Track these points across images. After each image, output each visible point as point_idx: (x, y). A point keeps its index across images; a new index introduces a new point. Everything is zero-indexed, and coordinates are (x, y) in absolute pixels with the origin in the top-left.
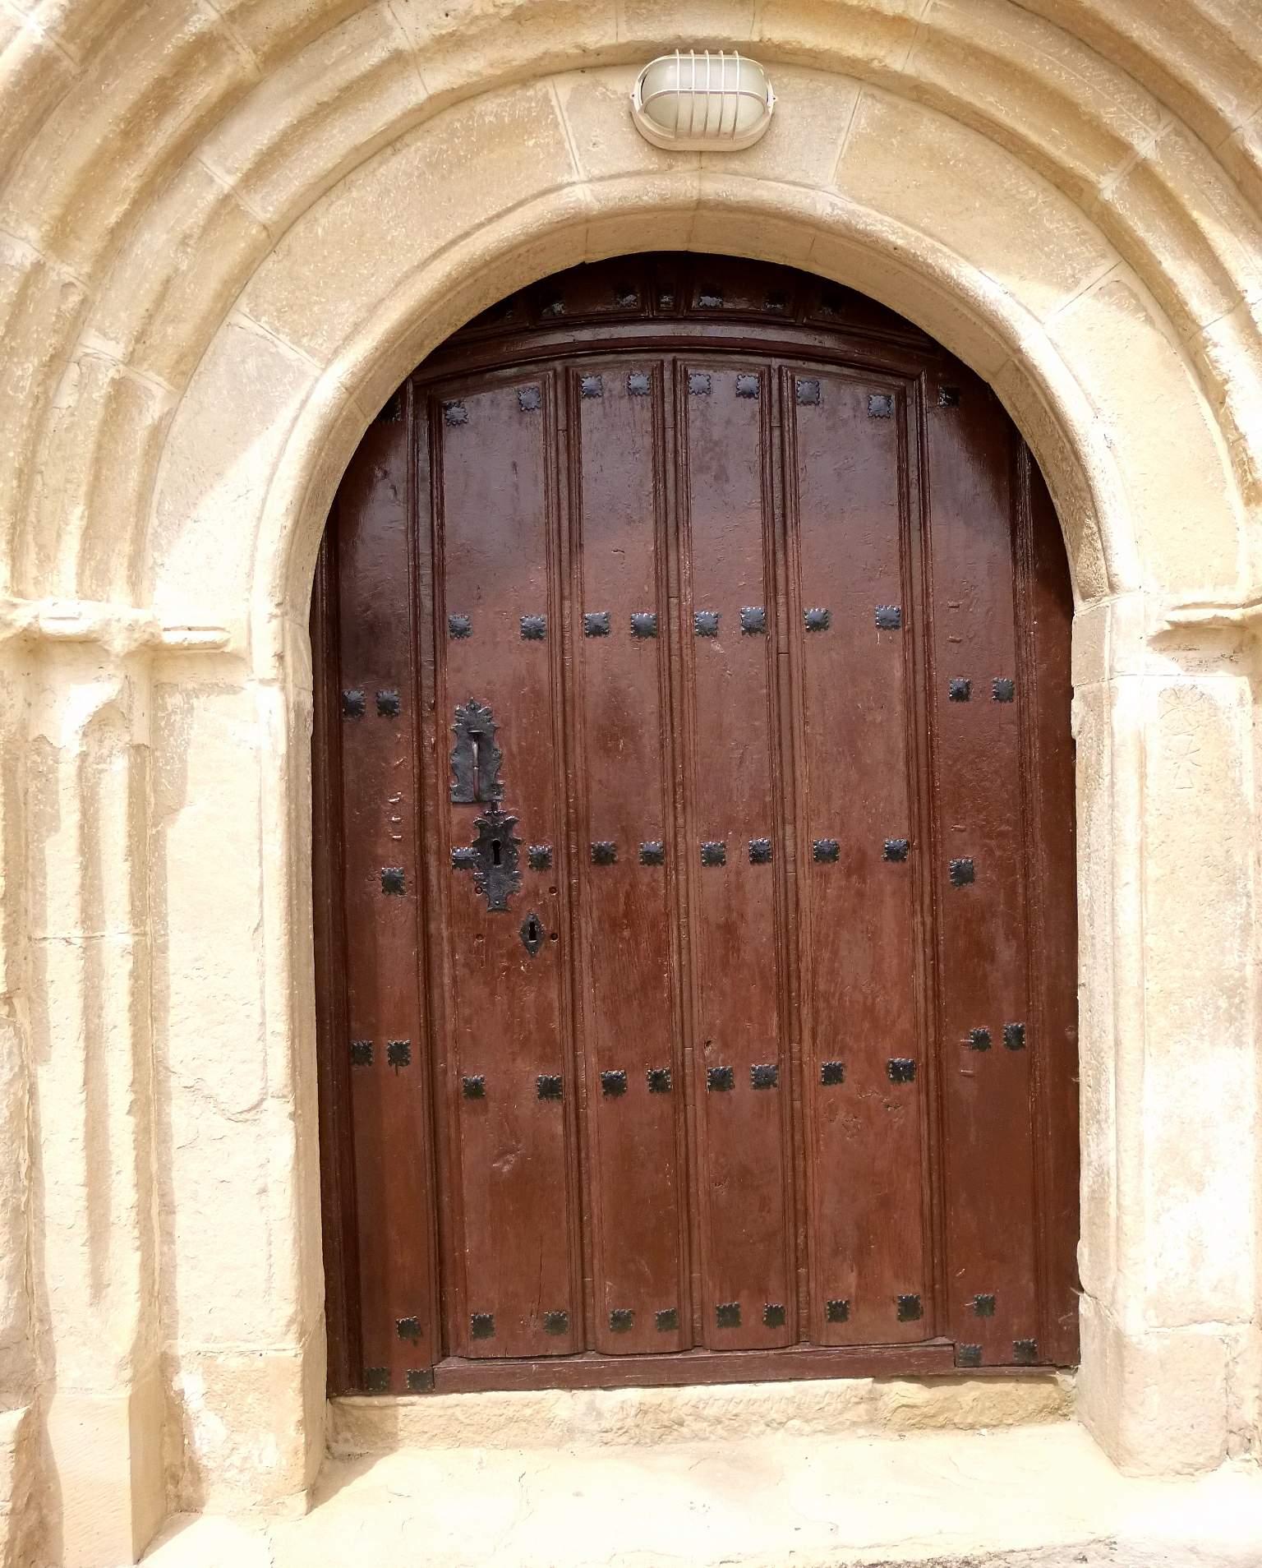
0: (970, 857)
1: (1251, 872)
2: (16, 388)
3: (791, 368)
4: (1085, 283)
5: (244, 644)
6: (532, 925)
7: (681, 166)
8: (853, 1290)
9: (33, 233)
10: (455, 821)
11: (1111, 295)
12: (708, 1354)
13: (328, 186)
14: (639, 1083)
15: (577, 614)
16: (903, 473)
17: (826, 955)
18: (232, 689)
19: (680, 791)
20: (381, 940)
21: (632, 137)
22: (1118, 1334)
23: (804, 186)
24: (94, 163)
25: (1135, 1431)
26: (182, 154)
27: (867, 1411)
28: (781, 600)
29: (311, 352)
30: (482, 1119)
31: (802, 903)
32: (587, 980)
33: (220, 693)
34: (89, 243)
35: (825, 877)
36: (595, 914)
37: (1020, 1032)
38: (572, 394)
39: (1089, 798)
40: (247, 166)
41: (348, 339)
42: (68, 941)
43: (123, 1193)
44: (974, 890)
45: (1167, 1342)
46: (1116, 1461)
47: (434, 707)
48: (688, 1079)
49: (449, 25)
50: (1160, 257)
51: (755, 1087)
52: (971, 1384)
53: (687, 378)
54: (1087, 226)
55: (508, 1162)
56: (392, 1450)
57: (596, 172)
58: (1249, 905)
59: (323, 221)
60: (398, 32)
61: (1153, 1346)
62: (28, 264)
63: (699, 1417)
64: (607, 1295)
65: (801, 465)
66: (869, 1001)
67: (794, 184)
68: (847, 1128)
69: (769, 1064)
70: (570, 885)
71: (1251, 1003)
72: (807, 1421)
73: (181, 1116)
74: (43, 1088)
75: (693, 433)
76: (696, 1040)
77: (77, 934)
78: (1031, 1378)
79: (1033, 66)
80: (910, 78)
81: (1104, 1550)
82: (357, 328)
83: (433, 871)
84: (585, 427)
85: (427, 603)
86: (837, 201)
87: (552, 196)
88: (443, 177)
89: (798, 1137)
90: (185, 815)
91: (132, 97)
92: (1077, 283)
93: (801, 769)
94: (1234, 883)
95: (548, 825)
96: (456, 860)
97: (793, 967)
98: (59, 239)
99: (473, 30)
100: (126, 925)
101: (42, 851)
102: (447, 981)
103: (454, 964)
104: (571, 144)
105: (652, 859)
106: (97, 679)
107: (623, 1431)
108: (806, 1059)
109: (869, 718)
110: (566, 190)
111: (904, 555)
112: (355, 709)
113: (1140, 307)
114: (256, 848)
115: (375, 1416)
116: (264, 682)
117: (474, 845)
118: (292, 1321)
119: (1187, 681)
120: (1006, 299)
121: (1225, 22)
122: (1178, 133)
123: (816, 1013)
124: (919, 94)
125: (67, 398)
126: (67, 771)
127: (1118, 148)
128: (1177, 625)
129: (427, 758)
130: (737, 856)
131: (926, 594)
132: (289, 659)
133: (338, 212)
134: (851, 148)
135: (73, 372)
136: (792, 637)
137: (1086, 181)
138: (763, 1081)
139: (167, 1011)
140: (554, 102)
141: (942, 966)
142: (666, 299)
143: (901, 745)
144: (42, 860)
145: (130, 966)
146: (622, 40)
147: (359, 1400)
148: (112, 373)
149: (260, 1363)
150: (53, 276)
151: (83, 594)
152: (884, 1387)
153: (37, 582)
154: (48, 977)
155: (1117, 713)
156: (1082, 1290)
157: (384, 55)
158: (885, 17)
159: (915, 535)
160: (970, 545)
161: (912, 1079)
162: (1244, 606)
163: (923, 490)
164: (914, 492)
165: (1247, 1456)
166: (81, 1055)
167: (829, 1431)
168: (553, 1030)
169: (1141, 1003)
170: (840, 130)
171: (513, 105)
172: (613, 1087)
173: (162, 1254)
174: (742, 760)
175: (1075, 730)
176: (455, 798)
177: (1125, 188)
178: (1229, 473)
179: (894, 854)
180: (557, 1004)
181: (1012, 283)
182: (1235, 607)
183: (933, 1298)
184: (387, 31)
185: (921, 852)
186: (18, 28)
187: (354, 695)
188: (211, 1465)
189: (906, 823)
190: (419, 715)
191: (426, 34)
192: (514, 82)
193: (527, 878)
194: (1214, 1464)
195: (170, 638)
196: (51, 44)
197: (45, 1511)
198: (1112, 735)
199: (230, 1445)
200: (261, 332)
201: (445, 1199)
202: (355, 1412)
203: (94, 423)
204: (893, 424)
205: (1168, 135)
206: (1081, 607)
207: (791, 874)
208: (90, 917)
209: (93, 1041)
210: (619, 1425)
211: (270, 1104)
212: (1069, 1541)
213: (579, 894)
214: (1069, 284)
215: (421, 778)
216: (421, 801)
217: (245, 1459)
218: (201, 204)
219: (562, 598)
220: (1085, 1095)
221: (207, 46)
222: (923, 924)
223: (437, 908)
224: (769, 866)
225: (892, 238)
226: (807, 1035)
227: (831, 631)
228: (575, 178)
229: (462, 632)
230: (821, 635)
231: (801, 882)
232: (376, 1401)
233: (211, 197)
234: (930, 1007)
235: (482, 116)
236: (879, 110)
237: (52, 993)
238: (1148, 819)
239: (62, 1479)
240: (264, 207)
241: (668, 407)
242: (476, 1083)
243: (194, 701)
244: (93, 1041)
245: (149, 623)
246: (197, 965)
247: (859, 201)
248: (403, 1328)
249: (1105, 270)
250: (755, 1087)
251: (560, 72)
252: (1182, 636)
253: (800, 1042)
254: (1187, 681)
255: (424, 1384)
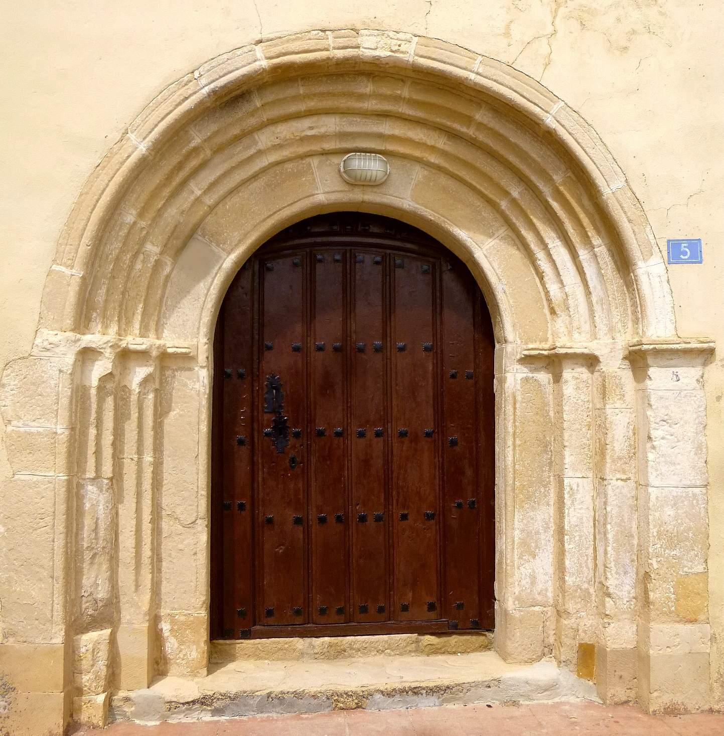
0: (455, 437)
1: (552, 444)
2: (124, 264)
3: (394, 254)
4: (496, 235)
5: (196, 353)
6: (293, 458)
7: (356, 190)
8: (411, 599)
9: (134, 212)
10: (266, 418)
11: (505, 239)
12: (356, 624)
13: (231, 192)
14: (332, 520)
15: (312, 342)
16: (434, 294)
17: (402, 472)
18: (190, 369)
19: (349, 409)
21: (339, 179)
22: (506, 611)
23: (400, 198)
24: (156, 189)
25: (511, 646)
26: (184, 183)
27: (416, 647)
28: (388, 339)
29: (224, 250)
30: (272, 532)
31: (394, 453)
32: (313, 479)
33: (185, 371)
34: (151, 214)
35: (402, 443)
36: (317, 455)
37: (473, 502)
38: (313, 261)
39: (499, 416)
40: (206, 187)
41: (237, 245)
42: (132, 459)
43: (147, 552)
44: (457, 449)
45: (522, 613)
46: (505, 659)
47: (258, 376)
48: (350, 518)
49: (278, 142)
50: (521, 230)
51: (375, 521)
52: (454, 636)
53: (356, 257)
54: (498, 216)
55: (281, 549)
56: (233, 661)
57: (326, 190)
58: (552, 455)
59: (229, 203)
60: (260, 143)
61: (517, 615)
62: (132, 222)
63: (352, 649)
64: (318, 600)
65: (396, 290)
66: (418, 490)
67: (396, 197)
68: (410, 538)
69: (380, 513)
70: (307, 444)
71: (552, 490)
72: (392, 651)
73: (165, 525)
74: (120, 512)
75: (358, 277)
76: (354, 503)
77: (135, 457)
78: (478, 634)
79: (478, 165)
80: (436, 164)
81: (496, 683)
82: (240, 241)
84: (317, 273)
85: (256, 337)
86: (410, 203)
87: (311, 198)
88: (272, 190)
89: (391, 541)
90: (172, 414)
91: (170, 167)
92: (494, 234)
93: (394, 403)
94: (547, 447)
96: (266, 433)
97: (390, 476)
98: (141, 215)
99: (286, 143)
100: (151, 454)
101: (124, 427)
102: (260, 479)
103: (263, 472)
104: (318, 180)
105: (339, 435)
106: (146, 366)
107: (323, 654)
108: (394, 511)
109: (420, 384)
110: (315, 196)
111: (434, 324)
112: (229, 376)
113: (515, 244)
114: (197, 427)
115: (227, 647)
116: (202, 367)
117: (272, 428)
118: (204, 603)
119: (530, 375)
120: (469, 240)
121: (539, 160)
122: (526, 189)
123: (398, 493)
124: (439, 168)
125: (139, 266)
126: (134, 398)
127: (507, 194)
128: (526, 356)
129: (255, 395)
130: (370, 435)
131: (441, 338)
132: (210, 358)
133: (235, 201)
134: (416, 185)
135: (141, 257)
136: (392, 353)
137: (496, 202)
138: (378, 519)
139: (162, 486)
140: (312, 165)
141: (445, 477)
142: (349, 227)
143: (432, 394)
144: (124, 430)
145: (152, 469)
146: (337, 147)
147: (221, 641)
148: (155, 258)
149: (191, 619)
150: (139, 225)
151: (142, 336)
152: (422, 637)
153: (125, 330)
154: (124, 472)
155: (507, 385)
156: (495, 600)
157: (255, 151)
158: (428, 146)
159: (438, 317)
160: (457, 322)
161: (433, 519)
162: (549, 350)
163: (441, 300)
164: (438, 301)
165: (551, 656)
166: (135, 500)
167: (401, 654)
169: (514, 490)
170: (412, 179)
171: (298, 166)
172: (322, 520)
173: (157, 577)
174: (372, 399)
175: (495, 390)
176: (266, 410)
177: (509, 205)
178: (545, 303)
179: (428, 435)
180: (301, 488)
181: (471, 234)
182: (545, 350)
183: (441, 604)
184: (256, 143)
185: (438, 434)
186: (137, 148)
187: (229, 371)
188: (172, 657)
189: (432, 424)
190: (252, 378)
191: (269, 144)
192: (298, 158)
193: (292, 441)
194: (539, 659)
195: (170, 350)
196: (147, 153)
197: (115, 669)
198: (505, 393)
199: (179, 650)
200: (206, 242)
201: (257, 563)
202: (220, 647)
203: (148, 275)
204: (430, 276)
205: (523, 190)
206: (497, 346)
207: (390, 442)
208: (140, 452)
209: (139, 495)
210: (321, 651)
211: (199, 522)
212: (484, 680)
213: (311, 448)
214: (491, 235)
215: (253, 403)
216: (252, 411)
217: (184, 655)
218: (189, 200)
219: (307, 336)
220: (497, 525)
221: (196, 150)
222: (439, 461)
223: (257, 452)
224: (382, 438)
225: (430, 217)
226: (395, 501)
227: (406, 352)
228: (319, 192)
229: (269, 348)
230: (403, 353)
231: (394, 444)
232: (228, 642)
233: (192, 198)
234: (441, 492)
235: (286, 169)
236: (426, 173)
237: (125, 477)
238: (517, 424)
239: (122, 657)
240: (209, 200)
241: (348, 267)
243: (176, 373)
244: (139, 495)
245: (164, 346)
246: (174, 469)
247: (418, 204)
248: (240, 613)
249: (503, 231)
250: (375, 521)
251: (314, 155)
252: (528, 360)
253: (392, 505)
254: (530, 375)
255: (247, 635)
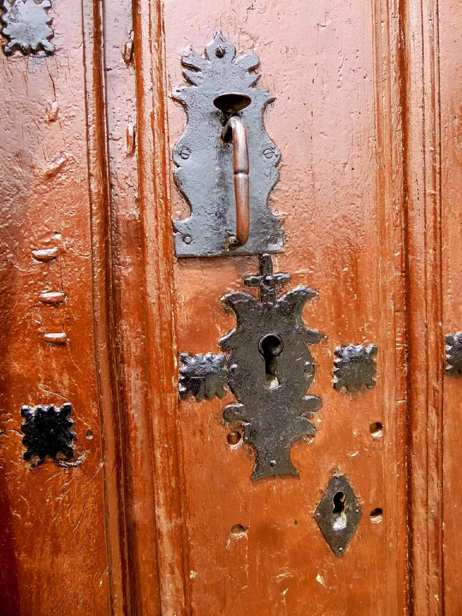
20: (27, 562)
83: (135, 399)
95: (369, 304)
117: (224, 346)
168: (283, 603)
242: (449, 337)
